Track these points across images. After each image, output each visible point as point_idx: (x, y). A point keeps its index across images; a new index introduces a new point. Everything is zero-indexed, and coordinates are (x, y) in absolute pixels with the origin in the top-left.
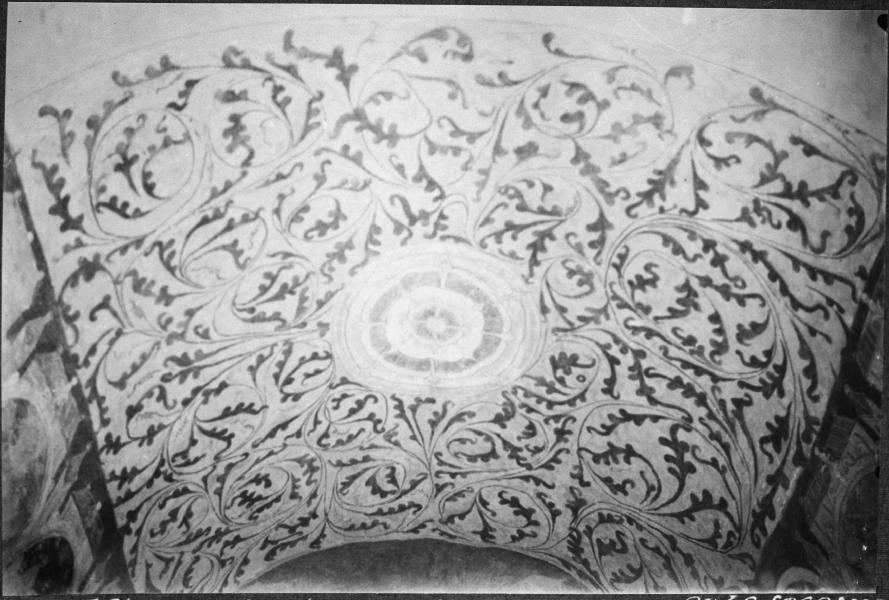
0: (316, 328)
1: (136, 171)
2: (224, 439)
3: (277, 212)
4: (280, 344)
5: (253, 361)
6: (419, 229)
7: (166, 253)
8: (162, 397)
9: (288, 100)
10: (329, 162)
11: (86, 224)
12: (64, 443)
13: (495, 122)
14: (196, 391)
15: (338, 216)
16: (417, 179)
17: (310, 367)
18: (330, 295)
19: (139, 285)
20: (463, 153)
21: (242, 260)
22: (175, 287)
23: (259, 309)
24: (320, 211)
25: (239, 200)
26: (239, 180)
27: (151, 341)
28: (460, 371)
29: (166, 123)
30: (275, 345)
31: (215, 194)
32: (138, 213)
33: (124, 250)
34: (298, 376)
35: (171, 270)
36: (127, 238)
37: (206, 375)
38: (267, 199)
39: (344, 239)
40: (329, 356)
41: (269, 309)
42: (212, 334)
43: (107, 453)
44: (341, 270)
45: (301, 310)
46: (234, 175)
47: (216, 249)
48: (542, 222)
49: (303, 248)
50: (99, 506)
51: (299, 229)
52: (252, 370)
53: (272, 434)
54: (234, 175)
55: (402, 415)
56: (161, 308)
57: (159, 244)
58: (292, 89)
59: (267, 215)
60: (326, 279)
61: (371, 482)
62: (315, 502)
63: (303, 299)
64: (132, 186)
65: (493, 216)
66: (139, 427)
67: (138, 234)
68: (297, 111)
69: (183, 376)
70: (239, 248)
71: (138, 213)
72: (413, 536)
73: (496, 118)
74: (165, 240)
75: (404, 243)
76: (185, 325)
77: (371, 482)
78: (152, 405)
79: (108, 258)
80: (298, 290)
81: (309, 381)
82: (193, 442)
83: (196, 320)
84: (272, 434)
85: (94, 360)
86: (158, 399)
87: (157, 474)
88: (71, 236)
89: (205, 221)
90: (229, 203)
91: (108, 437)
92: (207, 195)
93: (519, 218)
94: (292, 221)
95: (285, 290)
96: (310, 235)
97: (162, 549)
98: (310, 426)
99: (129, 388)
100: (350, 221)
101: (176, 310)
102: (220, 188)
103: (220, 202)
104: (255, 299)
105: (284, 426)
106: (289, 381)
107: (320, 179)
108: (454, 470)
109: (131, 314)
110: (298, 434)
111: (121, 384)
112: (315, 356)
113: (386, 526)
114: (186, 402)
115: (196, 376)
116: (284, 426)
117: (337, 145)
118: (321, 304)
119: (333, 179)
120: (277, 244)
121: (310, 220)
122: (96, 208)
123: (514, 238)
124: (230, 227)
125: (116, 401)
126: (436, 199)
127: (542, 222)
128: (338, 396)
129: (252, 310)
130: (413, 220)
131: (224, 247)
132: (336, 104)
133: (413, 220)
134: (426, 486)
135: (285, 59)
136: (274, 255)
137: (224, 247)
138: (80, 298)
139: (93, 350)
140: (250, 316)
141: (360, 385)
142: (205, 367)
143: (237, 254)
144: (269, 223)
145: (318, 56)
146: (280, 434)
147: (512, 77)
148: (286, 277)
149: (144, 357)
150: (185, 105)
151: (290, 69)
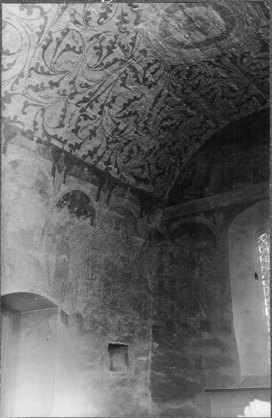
2: (134, 115)
8: (86, 117)
12: (49, 161)
14: (102, 107)
21: (77, 50)
23: (105, 62)
26: (46, 23)
27: (63, 103)
33: (17, 82)
36: (14, 77)
37: (102, 98)
41: (110, 58)
43: (75, 151)
45: (125, 51)
46: (42, 21)
47: (61, 54)
50: (86, 169)
54: (42, 21)
55: (215, 66)
57: (32, 69)
63: (122, 47)
67: (18, 72)
70: (71, 47)
74: (34, 65)
78: (83, 124)
79: (12, 90)
85: (39, 126)
89: (45, 48)
90: (50, 33)
91: (70, 146)
94: (87, 21)
96: (100, 22)
97: (241, 77)
99: (67, 125)
101: (63, 86)
102: (39, 30)
111: (61, 125)
113: (247, 109)
114: (100, 113)
124: (59, 43)
129: (102, 64)
131: (64, 51)
136: (91, 39)
137: (64, 51)
142: (98, 97)
148: (105, 44)
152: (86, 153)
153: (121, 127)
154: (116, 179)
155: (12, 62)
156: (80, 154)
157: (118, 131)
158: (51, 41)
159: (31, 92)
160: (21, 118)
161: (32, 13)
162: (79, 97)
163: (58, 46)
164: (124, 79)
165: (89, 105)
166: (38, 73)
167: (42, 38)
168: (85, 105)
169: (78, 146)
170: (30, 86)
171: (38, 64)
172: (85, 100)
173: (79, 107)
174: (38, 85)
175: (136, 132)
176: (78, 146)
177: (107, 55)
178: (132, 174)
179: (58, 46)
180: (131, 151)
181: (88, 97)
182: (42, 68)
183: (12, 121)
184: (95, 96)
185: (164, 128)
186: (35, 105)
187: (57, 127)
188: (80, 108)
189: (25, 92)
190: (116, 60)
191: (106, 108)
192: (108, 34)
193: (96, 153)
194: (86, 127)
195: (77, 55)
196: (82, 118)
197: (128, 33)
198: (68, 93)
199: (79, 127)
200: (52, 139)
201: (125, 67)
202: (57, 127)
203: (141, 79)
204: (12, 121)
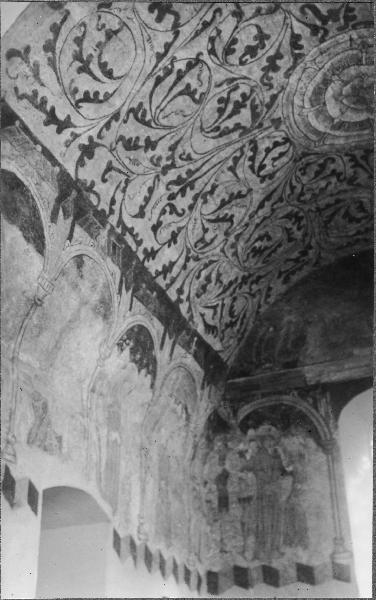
1: (94, 67)
4: (247, 145)
5: (230, 163)
8: (173, 209)
18: (274, 98)
21: (197, 97)
24: (247, 38)
25: (180, 54)
32: (108, 96)
35: (148, 124)
37: (199, 185)
39: (272, 52)
44: (277, 78)
46: (169, 37)
47: (175, 97)
51: (234, 59)
52: (232, 169)
56: (150, 153)
59: (205, 57)
63: (254, 108)
64: (95, 78)
69: (183, 192)
79: (99, 136)
80: (248, 103)
82: (205, 230)
83: (179, 150)
86: (171, 213)
87: (187, 259)
88: (67, 134)
89: (159, 81)
98: (288, 192)
100: (273, 38)
102: (162, 50)
103: (165, 62)
109: (131, 167)
114: (191, 208)
115: (192, 188)
121: (240, 48)
130: (324, 20)
131: (181, 93)
133: (324, 20)
137: (181, 93)
142: (196, 179)
144: (209, 62)
160: (99, 187)
162: (172, 175)
167: (160, 65)
179: (175, 84)
182: (144, 115)
190: (238, 126)
192: (245, 81)
195: (193, 104)
197: (271, 87)
198: (164, 163)
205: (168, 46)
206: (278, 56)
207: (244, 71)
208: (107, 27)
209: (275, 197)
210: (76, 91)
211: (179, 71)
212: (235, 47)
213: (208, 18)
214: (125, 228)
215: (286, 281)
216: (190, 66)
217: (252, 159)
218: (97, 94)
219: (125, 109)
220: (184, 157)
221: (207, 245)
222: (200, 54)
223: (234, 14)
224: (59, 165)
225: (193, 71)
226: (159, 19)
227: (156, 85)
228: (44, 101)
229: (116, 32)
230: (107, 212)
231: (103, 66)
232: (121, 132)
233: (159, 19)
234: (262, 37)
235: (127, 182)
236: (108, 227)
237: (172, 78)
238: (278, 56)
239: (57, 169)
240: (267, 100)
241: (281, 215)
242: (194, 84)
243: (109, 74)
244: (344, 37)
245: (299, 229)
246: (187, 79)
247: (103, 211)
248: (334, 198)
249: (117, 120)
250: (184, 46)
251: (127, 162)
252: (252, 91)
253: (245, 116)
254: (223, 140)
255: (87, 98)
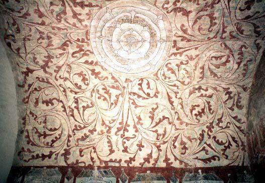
0: (127, 83)
1: (48, 132)
3: (76, 93)
5: (133, 106)
6: (86, 48)
7: (78, 128)
8: (128, 139)
9: (39, 87)
10: (60, 76)
11: (53, 151)
13: (32, 26)
14: (135, 127)
15: (80, 74)
16: (64, 50)
17: (144, 86)
18: (113, 78)
19: (83, 139)
20: (49, 35)
21: (90, 105)
22: (90, 128)
24: (78, 80)
25: (70, 104)
26: (63, 104)
28: (18, 106)
29: (39, 121)
30: (129, 98)
31: (65, 111)
32: (60, 135)
34: (147, 91)
35: (85, 127)
37: (131, 123)
38: (71, 96)
39: (90, 72)
40: (142, 80)
41: (113, 98)
42: (114, 118)
43: (131, 163)
44: (103, 74)
45: (117, 88)
46: (61, 104)
47: (83, 113)
48: (69, 4)
49: (91, 86)
51: (84, 87)
52: (136, 106)
53: (171, 103)
54: (61, 104)
56: (96, 133)
58: (36, 85)
59: (77, 96)
60: (106, 80)
61: (218, 67)
62: (219, 88)
63: (113, 87)
64: (51, 135)
65: (71, 23)
66: (134, 148)
68: (43, 85)
69: (126, 130)
70: (86, 106)
71: (60, 135)
72: (261, 51)
73: (30, 25)
75: (92, 53)
76: (107, 126)
77: (218, 67)
78: (128, 144)
79: (68, 146)
80: (108, 88)
81: (151, 87)
82: (156, 131)
83: (107, 123)
84: (171, 103)
86: (128, 140)
87: (158, 147)
88: (54, 156)
89: (73, 116)
92: (65, 113)
93: (70, 13)
95: (107, 92)
98: (175, 88)
100: (83, 70)
102: (63, 109)
103: (68, 110)
104: (108, 103)
105: (170, 98)
106: (148, 94)
107: (66, 79)
108: (221, 31)
109: (91, 143)
110: (176, 93)
111: (112, 151)
112: (140, 84)
114: (137, 131)
115: (129, 126)
116: (170, 98)
117: (54, 74)
118: (117, 81)
119: (66, 75)
120: (88, 94)
121: (80, 83)
122: (51, 146)
123: (80, 14)
125: (118, 155)
126: (71, 43)
127: (69, 4)
128: (163, 78)
130: (81, 50)
131: (84, 110)
132: (40, 73)
133: (81, 50)
134: (229, 43)
135: (26, 87)
137: (84, 110)
138: (72, 160)
139: (92, 159)
140: (114, 105)
141: (159, 69)
142: (126, 122)
143: (88, 107)
144: (79, 96)
145: (25, 78)
146: (174, 99)
147: (12, 22)
149: (109, 142)
150: (36, 115)
151: (30, 86)
152: (142, 161)
153: (161, 131)
154: (182, 169)
155: (60, 133)
156: (136, 164)
157: (161, 135)
158: (73, 110)
159: (80, 142)
160: (81, 159)
161: (53, 104)
163: (78, 111)
164: (134, 103)
165: (124, 130)
166: (79, 130)
167: (68, 112)
168: (121, 132)
169: (132, 159)
170: (78, 140)
171: (75, 126)
172: (119, 130)
173: (118, 135)
174: (82, 137)
175: (177, 129)
176: (132, 159)
177: (110, 97)
178: (197, 158)
179: (78, 111)
180: (182, 143)
181: (120, 126)
182: (80, 126)
183: (76, 164)
184: (125, 123)
185: (200, 114)
186: (88, 148)
187: (109, 154)
188: (120, 136)
189: (77, 144)
190: (117, 96)
191: (139, 126)
192: (97, 86)
193: (151, 157)
194: (132, 144)
196: (125, 140)
197: (107, 78)
198: (105, 130)
199: (127, 147)
200: (109, 163)
201: (127, 96)
202: (109, 154)
203: (146, 97)
204: (76, 164)
205: (64, 107)
206: (93, 71)
207: (91, 86)
208: (42, 121)
209: (173, 95)
210: (48, 143)
211: (75, 107)
212: (79, 84)
213: (62, 89)
214: (106, 162)
215: (240, 107)
216: (77, 102)
217: (139, 96)
218: (56, 138)
219: (71, 131)
220: (112, 122)
221: (164, 135)
222: (74, 97)
223: (65, 80)
224: (56, 166)
225: (79, 102)
226: (53, 104)
227: (73, 117)
228: (38, 155)
229: (46, 119)
230: (92, 164)
231: (51, 130)
232: (76, 138)
233: (53, 104)
234: (80, 74)
235: (94, 148)
236: (96, 168)
237: (76, 111)
238: (93, 71)
239: (57, 169)
240: (113, 81)
241: (187, 96)
242: (85, 105)
243: (55, 129)
244: (93, 44)
245: (207, 90)
246: (80, 106)
247: (90, 165)
248: (198, 68)
249: (71, 137)
250: (68, 101)
251: (88, 143)
252: (104, 85)
253: (114, 92)
254: (119, 104)
255: (53, 141)
